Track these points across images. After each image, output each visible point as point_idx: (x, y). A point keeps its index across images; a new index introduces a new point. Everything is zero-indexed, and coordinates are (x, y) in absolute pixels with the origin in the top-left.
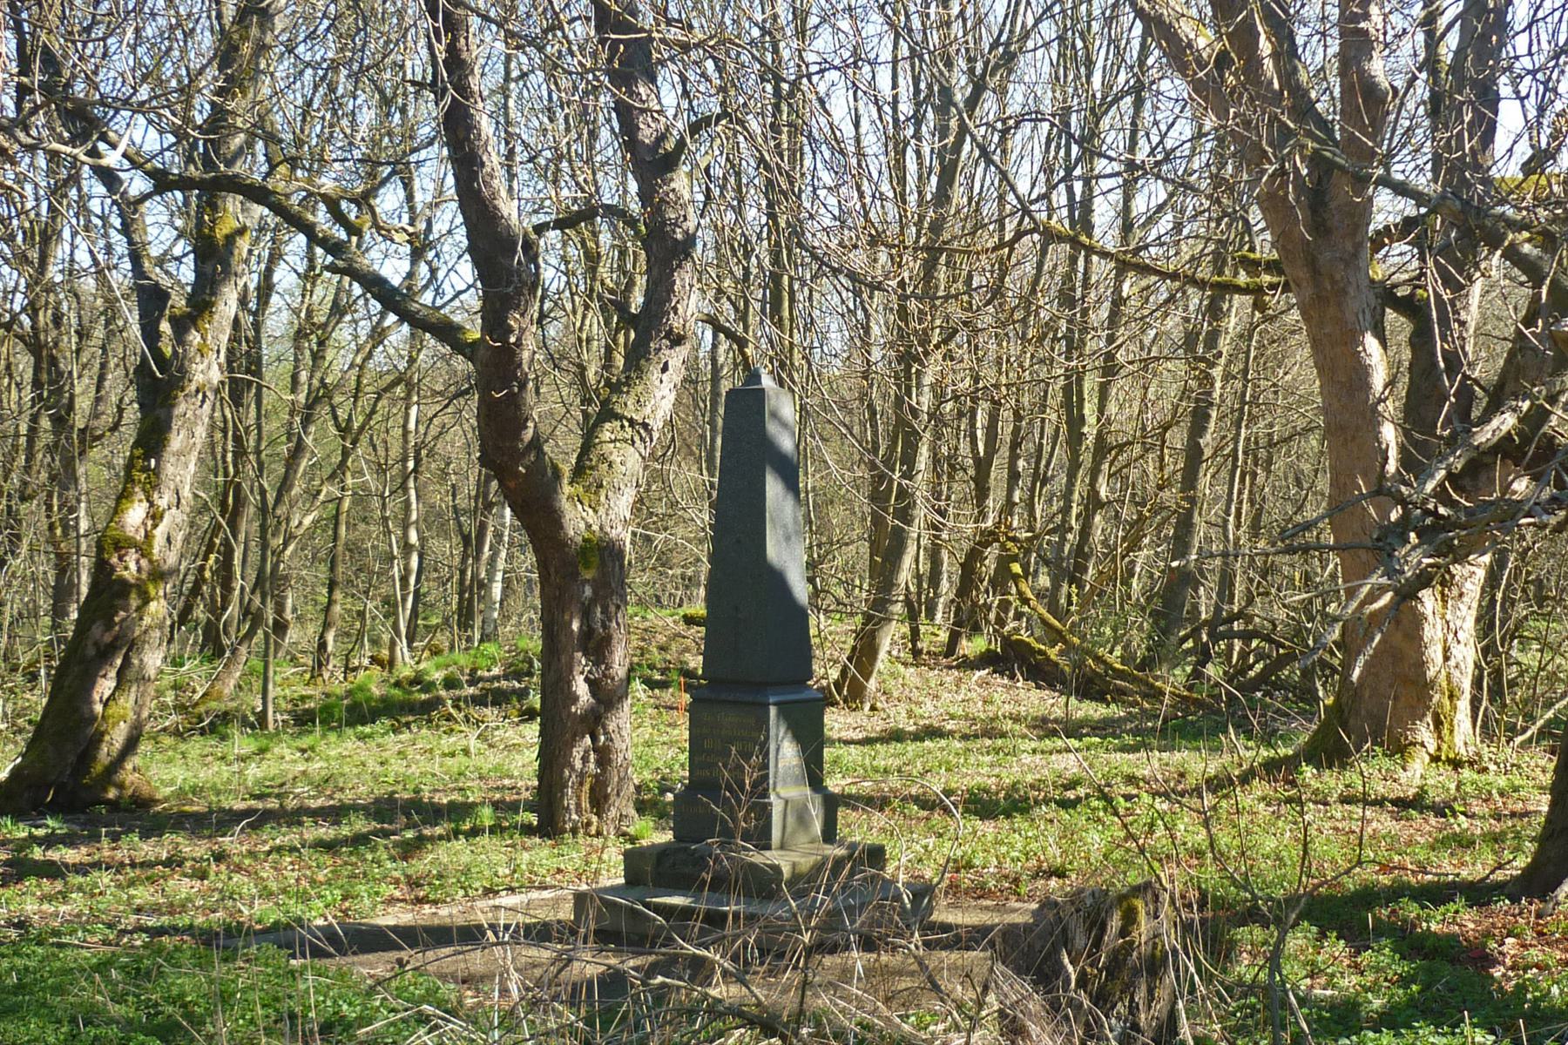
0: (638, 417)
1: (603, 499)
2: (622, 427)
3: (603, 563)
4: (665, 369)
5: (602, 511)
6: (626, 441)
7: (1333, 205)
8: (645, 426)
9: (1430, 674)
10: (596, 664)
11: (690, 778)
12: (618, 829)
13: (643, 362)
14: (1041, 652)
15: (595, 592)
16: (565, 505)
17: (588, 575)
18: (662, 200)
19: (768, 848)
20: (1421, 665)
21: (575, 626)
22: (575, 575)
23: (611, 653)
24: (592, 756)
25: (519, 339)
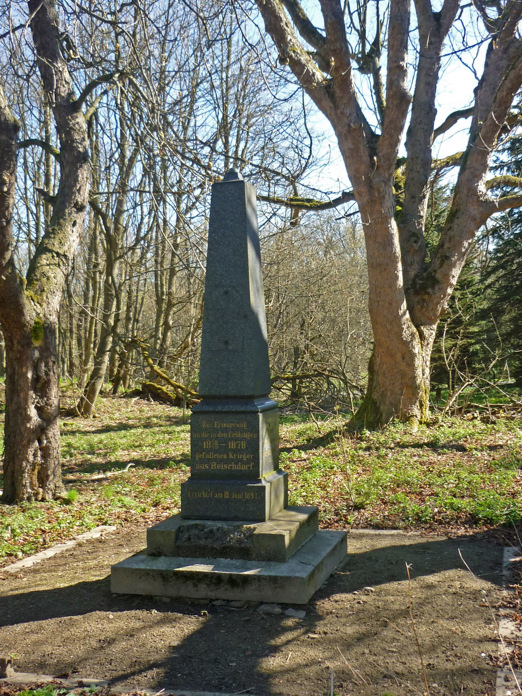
0: (61, 252)
1: (45, 298)
2: (53, 257)
3: (46, 337)
5: (45, 305)
6: (55, 264)
8: (65, 256)
9: (418, 382)
10: (41, 397)
11: (192, 472)
12: (54, 495)
13: (61, 221)
14: (160, 389)
15: (41, 354)
16: (26, 301)
17: (37, 344)
18: (71, 128)
19: (263, 520)
20: (414, 378)
21: (30, 375)
22: (29, 344)
23: (50, 390)
24: (39, 453)
25: (9, 190)
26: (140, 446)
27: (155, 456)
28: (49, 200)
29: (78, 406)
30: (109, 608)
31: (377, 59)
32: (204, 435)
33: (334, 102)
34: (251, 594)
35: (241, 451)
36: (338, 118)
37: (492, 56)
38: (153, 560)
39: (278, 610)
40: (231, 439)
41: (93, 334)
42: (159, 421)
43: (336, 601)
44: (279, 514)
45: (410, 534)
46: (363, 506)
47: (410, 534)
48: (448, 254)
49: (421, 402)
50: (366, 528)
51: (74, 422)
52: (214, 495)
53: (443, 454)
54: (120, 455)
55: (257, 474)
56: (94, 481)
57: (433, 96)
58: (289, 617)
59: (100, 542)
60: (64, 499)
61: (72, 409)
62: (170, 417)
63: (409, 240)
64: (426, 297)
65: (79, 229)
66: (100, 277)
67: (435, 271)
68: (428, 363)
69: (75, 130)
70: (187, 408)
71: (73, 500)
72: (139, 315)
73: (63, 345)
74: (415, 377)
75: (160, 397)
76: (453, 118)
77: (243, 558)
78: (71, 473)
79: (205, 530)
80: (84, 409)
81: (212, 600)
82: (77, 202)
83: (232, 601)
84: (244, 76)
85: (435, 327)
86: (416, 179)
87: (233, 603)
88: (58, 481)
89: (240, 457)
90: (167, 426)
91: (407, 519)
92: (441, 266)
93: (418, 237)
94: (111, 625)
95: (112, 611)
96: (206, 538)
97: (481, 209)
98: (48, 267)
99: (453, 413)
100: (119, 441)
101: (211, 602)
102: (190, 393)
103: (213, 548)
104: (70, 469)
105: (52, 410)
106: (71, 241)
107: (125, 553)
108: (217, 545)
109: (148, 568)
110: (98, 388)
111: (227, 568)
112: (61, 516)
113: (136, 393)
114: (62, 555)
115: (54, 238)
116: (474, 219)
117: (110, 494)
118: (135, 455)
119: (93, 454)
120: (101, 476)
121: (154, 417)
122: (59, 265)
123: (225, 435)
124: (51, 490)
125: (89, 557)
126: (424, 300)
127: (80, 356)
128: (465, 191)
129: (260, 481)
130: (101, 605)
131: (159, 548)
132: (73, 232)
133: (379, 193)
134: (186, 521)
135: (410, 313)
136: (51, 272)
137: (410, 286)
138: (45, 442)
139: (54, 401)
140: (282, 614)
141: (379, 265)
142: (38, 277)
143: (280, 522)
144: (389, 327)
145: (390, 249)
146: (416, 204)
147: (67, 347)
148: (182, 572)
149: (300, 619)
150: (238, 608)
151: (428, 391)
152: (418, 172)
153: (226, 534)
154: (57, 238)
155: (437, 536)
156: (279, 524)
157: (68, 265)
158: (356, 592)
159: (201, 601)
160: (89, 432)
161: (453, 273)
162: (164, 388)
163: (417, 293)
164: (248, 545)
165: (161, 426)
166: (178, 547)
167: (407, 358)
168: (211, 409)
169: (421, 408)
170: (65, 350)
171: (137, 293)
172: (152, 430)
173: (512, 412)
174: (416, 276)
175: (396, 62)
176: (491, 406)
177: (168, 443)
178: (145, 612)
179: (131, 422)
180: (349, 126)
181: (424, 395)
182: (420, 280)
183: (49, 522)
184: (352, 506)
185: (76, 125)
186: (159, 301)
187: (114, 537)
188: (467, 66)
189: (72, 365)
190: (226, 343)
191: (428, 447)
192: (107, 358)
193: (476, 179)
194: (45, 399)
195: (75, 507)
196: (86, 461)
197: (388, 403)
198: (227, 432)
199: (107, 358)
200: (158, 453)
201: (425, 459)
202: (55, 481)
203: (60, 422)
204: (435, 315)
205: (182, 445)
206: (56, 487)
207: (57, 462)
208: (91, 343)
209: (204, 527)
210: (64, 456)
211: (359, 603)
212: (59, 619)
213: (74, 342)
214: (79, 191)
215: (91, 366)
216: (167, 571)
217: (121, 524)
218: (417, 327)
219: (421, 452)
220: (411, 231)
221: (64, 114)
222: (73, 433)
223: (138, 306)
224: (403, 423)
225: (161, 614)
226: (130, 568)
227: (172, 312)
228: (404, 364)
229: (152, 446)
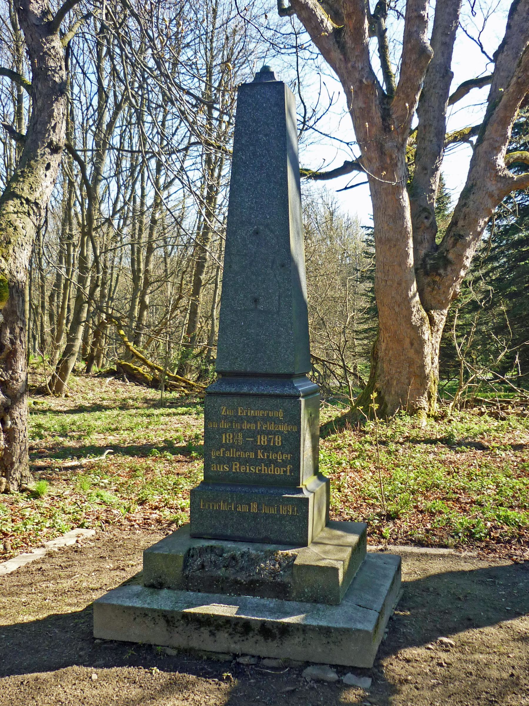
0: (32, 198)
1: (11, 251)
2: (22, 203)
3: (12, 297)
4: (48, 167)
5: (11, 260)
6: (24, 213)
7: (394, 116)
8: (36, 204)
9: (427, 371)
10: (6, 370)
12: (20, 486)
13: (32, 162)
14: (136, 369)
18: (46, 53)
23: (16, 362)
26: (116, 429)
27: (134, 442)
28: (19, 138)
29: (50, 384)
30: (90, 662)
31: (383, 19)
32: (224, 425)
33: (345, 54)
34: (291, 649)
35: (275, 449)
36: (349, 73)
37: (516, 17)
38: (152, 594)
39: (332, 676)
40: (262, 432)
41: (66, 310)
42: (135, 403)
43: (408, 661)
44: (323, 534)
45: (463, 554)
46: (398, 515)
47: (463, 554)
48: (462, 233)
49: (429, 393)
50: (406, 544)
51: (45, 401)
52: (235, 508)
53: (462, 452)
54: (95, 439)
55: (297, 481)
56: (66, 469)
57: (450, 58)
58: (348, 687)
59: (76, 551)
60: (31, 491)
61: (43, 387)
62: (146, 399)
63: (420, 215)
64: (437, 279)
65: (53, 174)
66: (74, 250)
67: (448, 251)
68: (437, 351)
69: (50, 56)
70: (166, 390)
71: (43, 493)
72: (113, 294)
73: (35, 321)
74: (424, 365)
75: (136, 378)
76: (466, 87)
77: (278, 597)
78: (41, 457)
79: (225, 555)
80: (56, 387)
81: (236, 656)
82: (52, 141)
83: (264, 658)
84: (230, 45)
85: (445, 312)
86: (428, 148)
87: (266, 662)
88: (25, 469)
89: (272, 456)
90: (144, 408)
91: (457, 534)
92: (454, 244)
93: (430, 213)
94: (95, 692)
95: (95, 667)
96: (226, 567)
97: (499, 185)
98: (16, 215)
99: (461, 407)
100: (92, 423)
101: (235, 659)
102: (168, 375)
103: (236, 582)
104: (40, 453)
105: (18, 386)
106: (44, 187)
107: (110, 579)
108: (242, 578)
109: (146, 606)
110: (71, 366)
111: (260, 611)
112: (28, 514)
113: (110, 373)
114: (27, 570)
115: (24, 181)
116: (491, 196)
117: (86, 486)
118: (112, 439)
119: (66, 436)
120: (75, 463)
121: (130, 398)
122: (29, 215)
123: (253, 427)
124: (16, 480)
125: (62, 574)
126: (434, 282)
127: (52, 331)
128: (482, 165)
129: (300, 491)
130: (80, 656)
131: (160, 577)
132: (46, 176)
133: (392, 159)
135: (419, 295)
136: (18, 221)
137: (419, 266)
138: (9, 423)
139: (22, 376)
140: (339, 681)
141: (389, 240)
142: (3, 227)
143: (328, 548)
144: (397, 309)
145: (401, 223)
146: (428, 176)
147: (39, 323)
148: (195, 614)
149: (365, 690)
150: (273, 668)
151: (436, 381)
152: (431, 141)
153: (254, 561)
154: (27, 183)
155: (499, 560)
156: (325, 551)
157: (40, 215)
158: (430, 646)
159: (221, 656)
160: (61, 412)
161: (467, 254)
162: (140, 369)
163: (427, 274)
164: (286, 580)
165: (137, 408)
166: (187, 577)
167: (416, 344)
168: (233, 390)
169: (429, 399)
170: (37, 326)
171: (112, 270)
172: (128, 412)
173: (522, 408)
174: (426, 255)
175: (416, 10)
176: (500, 401)
177: (147, 427)
178: (143, 671)
179: (105, 403)
180: (361, 82)
181: (433, 385)
182: (431, 259)
183: (13, 521)
184: (384, 515)
185: (52, 50)
186: (136, 279)
187: (93, 544)
188: (473, 39)
189: (43, 341)
190: (256, 301)
191: (442, 443)
192: (81, 329)
193: (495, 152)
194: (10, 372)
195: (44, 503)
196: (58, 444)
197: (393, 393)
198: (256, 423)
199: (81, 329)
200: (138, 438)
201: (443, 457)
202: (22, 468)
203: (28, 401)
204: (447, 299)
205: (163, 430)
206: (22, 476)
207: (23, 448)
208: (64, 318)
209: (223, 551)
210: (33, 438)
211: (441, 665)
212: (20, 677)
213: (46, 318)
214: (54, 128)
215: (63, 343)
216: (172, 611)
217: (101, 527)
218: (427, 311)
219: (436, 449)
220: (421, 206)
221: (37, 35)
222: (44, 412)
223: (113, 284)
224: (411, 415)
225: (165, 674)
226: (121, 606)
227: (148, 291)
228: (412, 351)
229: (131, 429)
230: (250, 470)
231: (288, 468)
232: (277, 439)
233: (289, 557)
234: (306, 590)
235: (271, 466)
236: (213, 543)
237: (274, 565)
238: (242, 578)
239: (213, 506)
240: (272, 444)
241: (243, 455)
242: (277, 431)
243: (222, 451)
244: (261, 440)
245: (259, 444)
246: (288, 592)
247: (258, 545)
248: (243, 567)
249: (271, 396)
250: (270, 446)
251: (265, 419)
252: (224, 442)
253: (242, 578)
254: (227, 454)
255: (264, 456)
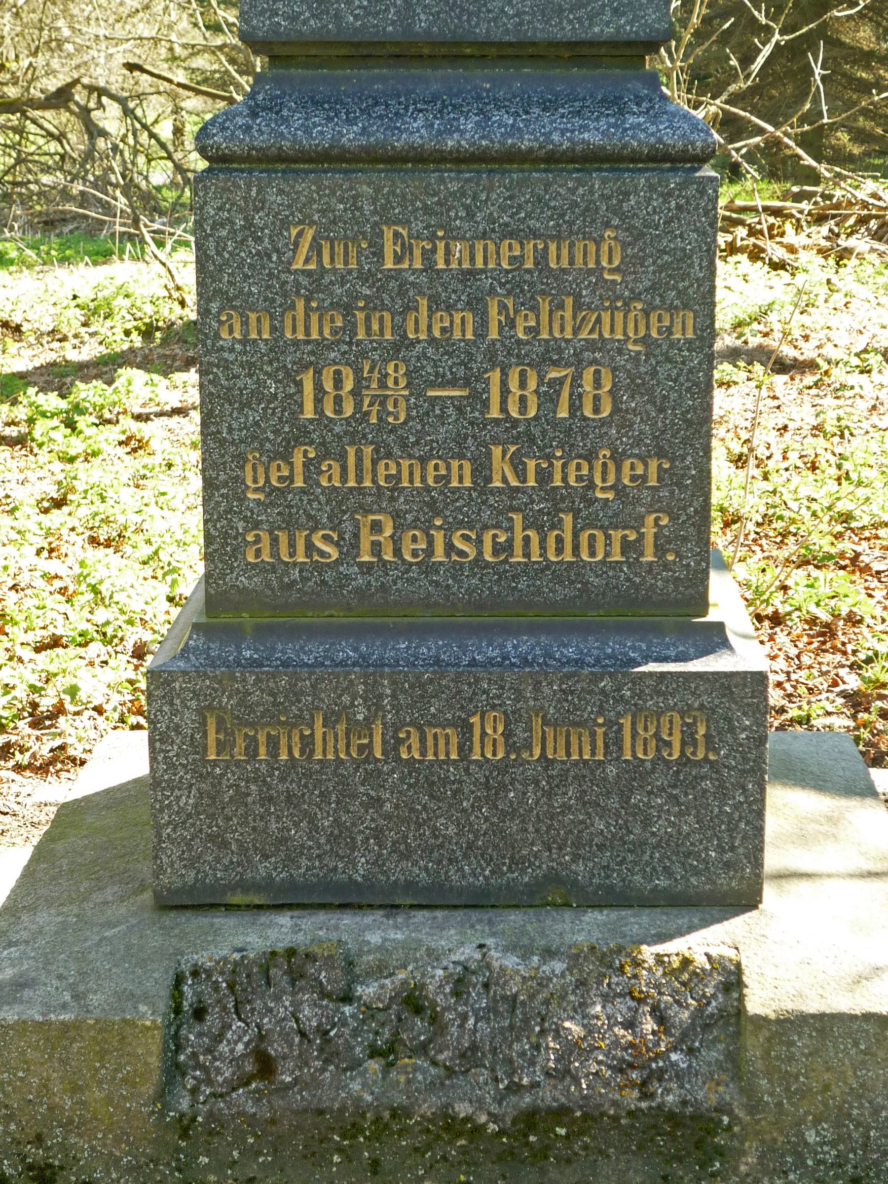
32: (305, 325)
35: (577, 438)
52: (392, 746)
89: (567, 474)
96: (386, 1053)
103: (450, 1125)
123: (462, 325)
134: (195, 923)
164: (707, 1095)
166: (185, 1127)
168: (350, 136)
198: (477, 305)
230: (450, 547)
231: (649, 530)
232: (514, 385)
233: (699, 976)
234: (811, 1137)
235: (557, 525)
236: (283, 930)
237: (630, 1025)
238: (480, 1103)
239: (273, 744)
240: (563, 413)
241: (412, 475)
242: (591, 345)
243: (298, 459)
244: (505, 392)
245: (495, 413)
246: (720, 1152)
247: (515, 918)
248: (474, 1047)
249: (553, 159)
250: (555, 424)
251: (522, 287)
252: (309, 412)
253: (480, 1103)
254: (330, 476)
255: (522, 476)
